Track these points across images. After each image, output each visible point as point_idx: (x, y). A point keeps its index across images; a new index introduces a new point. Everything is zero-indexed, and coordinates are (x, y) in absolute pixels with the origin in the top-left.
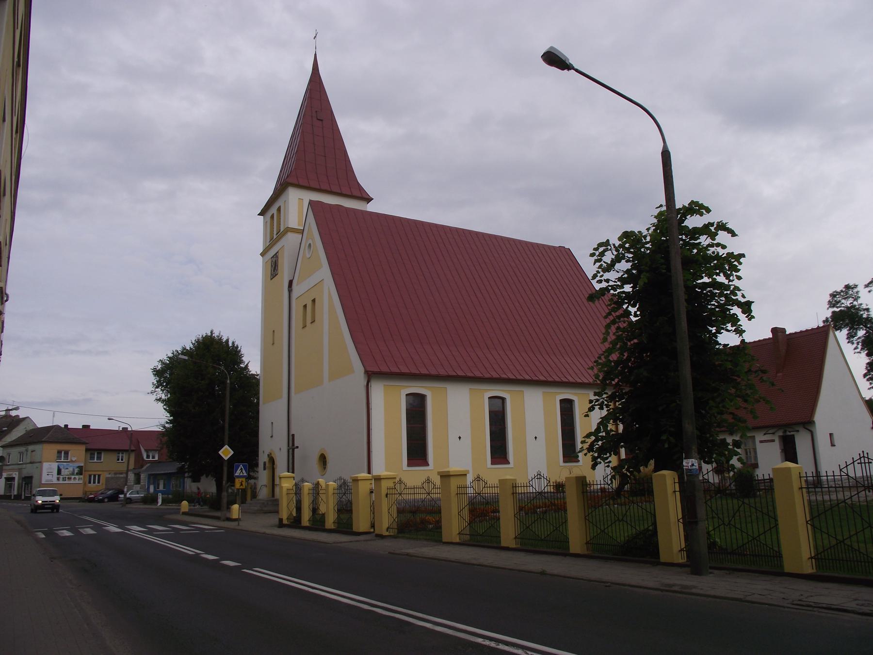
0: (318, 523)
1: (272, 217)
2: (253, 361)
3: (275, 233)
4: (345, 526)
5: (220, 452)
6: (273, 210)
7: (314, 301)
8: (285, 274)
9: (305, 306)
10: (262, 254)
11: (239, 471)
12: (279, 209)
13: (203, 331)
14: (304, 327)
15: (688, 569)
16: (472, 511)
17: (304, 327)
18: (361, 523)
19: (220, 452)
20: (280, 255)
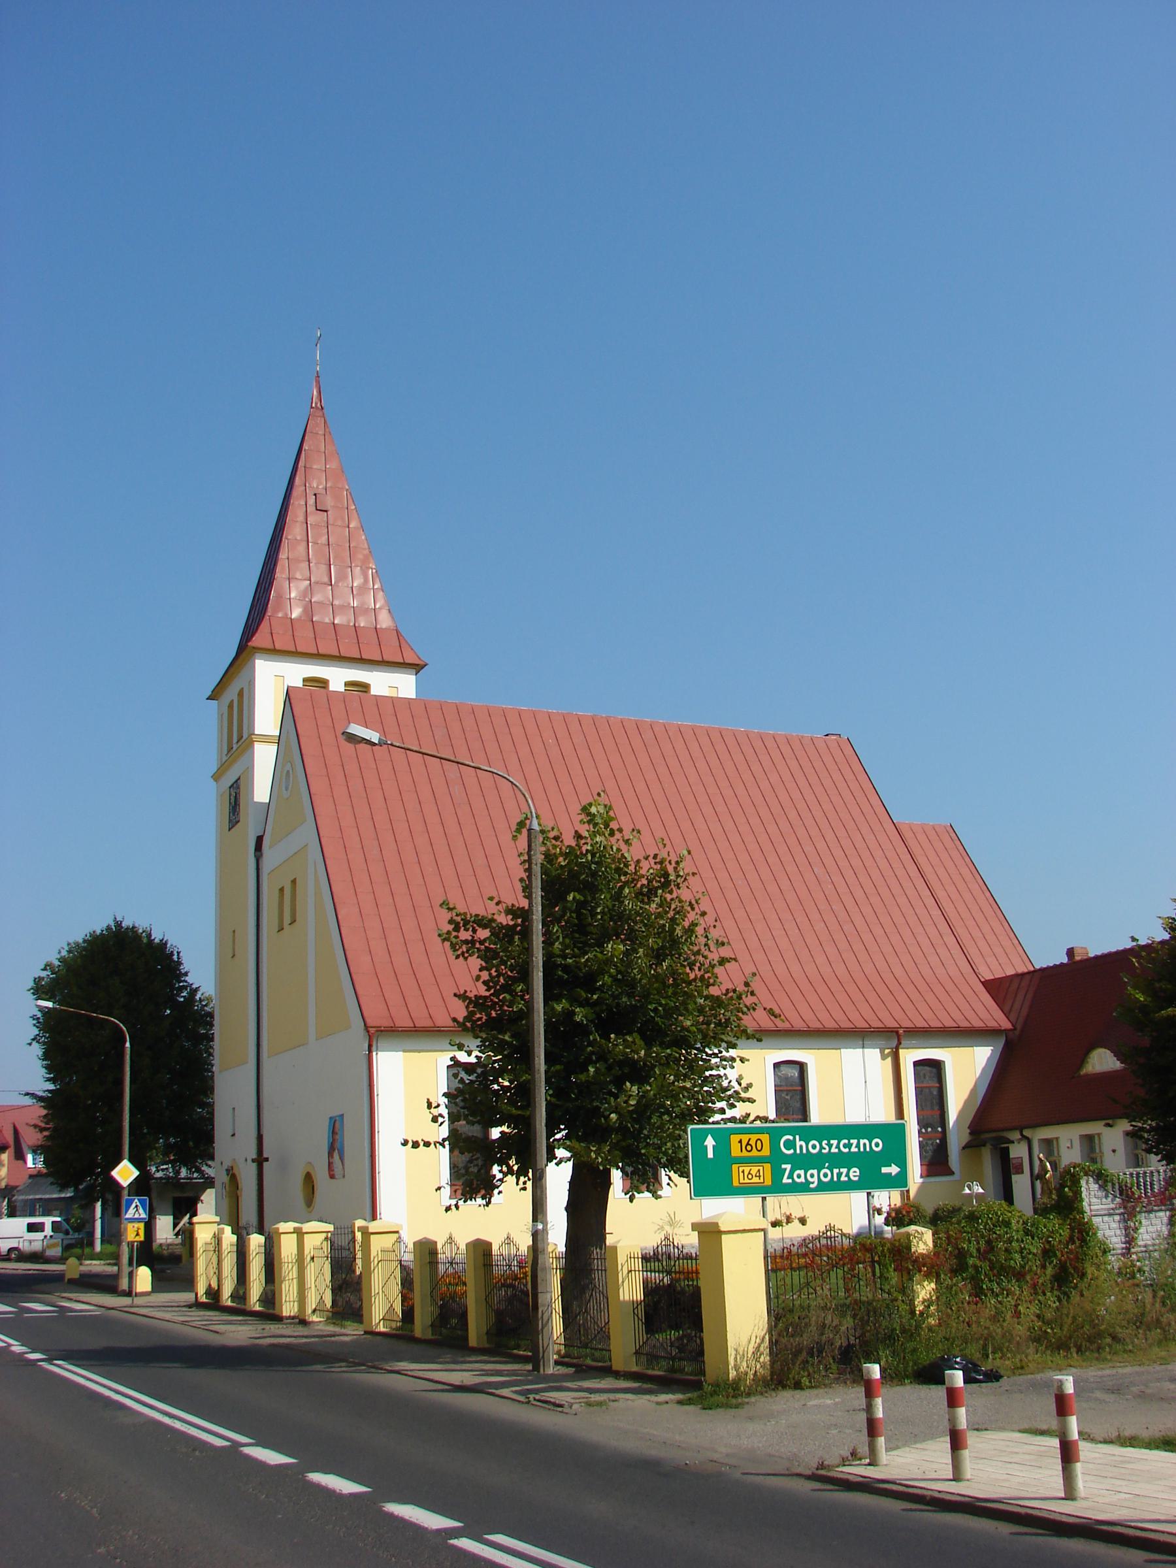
0: (239, 1308)
1: (231, 706)
2: (201, 973)
3: (235, 740)
4: (270, 1312)
5: (114, 1173)
6: (231, 694)
7: (294, 882)
8: (250, 828)
9: (282, 890)
10: (217, 777)
11: (132, 1211)
12: (241, 694)
13: (99, 923)
14: (281, 929)
15: (51, 1180)
16: (665, 1383)
17: (281, 929)
18: (289, 1308)
19: (114, 1173)
20: (242, 782)
